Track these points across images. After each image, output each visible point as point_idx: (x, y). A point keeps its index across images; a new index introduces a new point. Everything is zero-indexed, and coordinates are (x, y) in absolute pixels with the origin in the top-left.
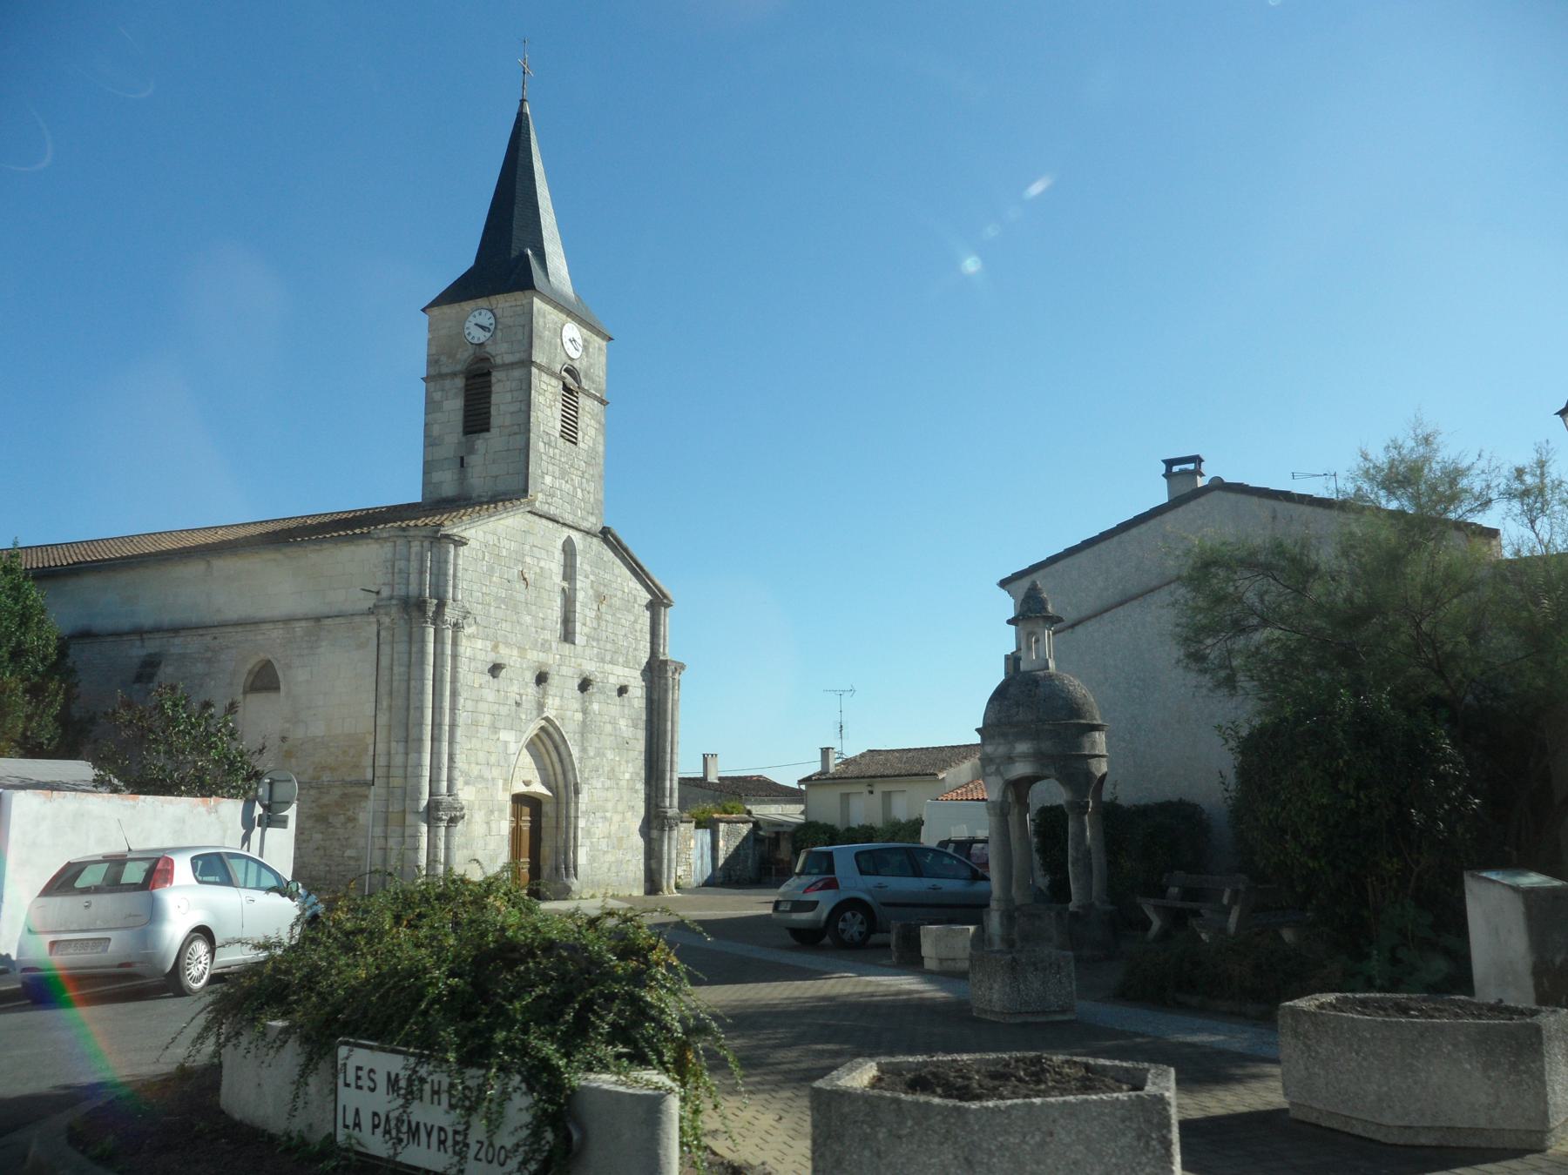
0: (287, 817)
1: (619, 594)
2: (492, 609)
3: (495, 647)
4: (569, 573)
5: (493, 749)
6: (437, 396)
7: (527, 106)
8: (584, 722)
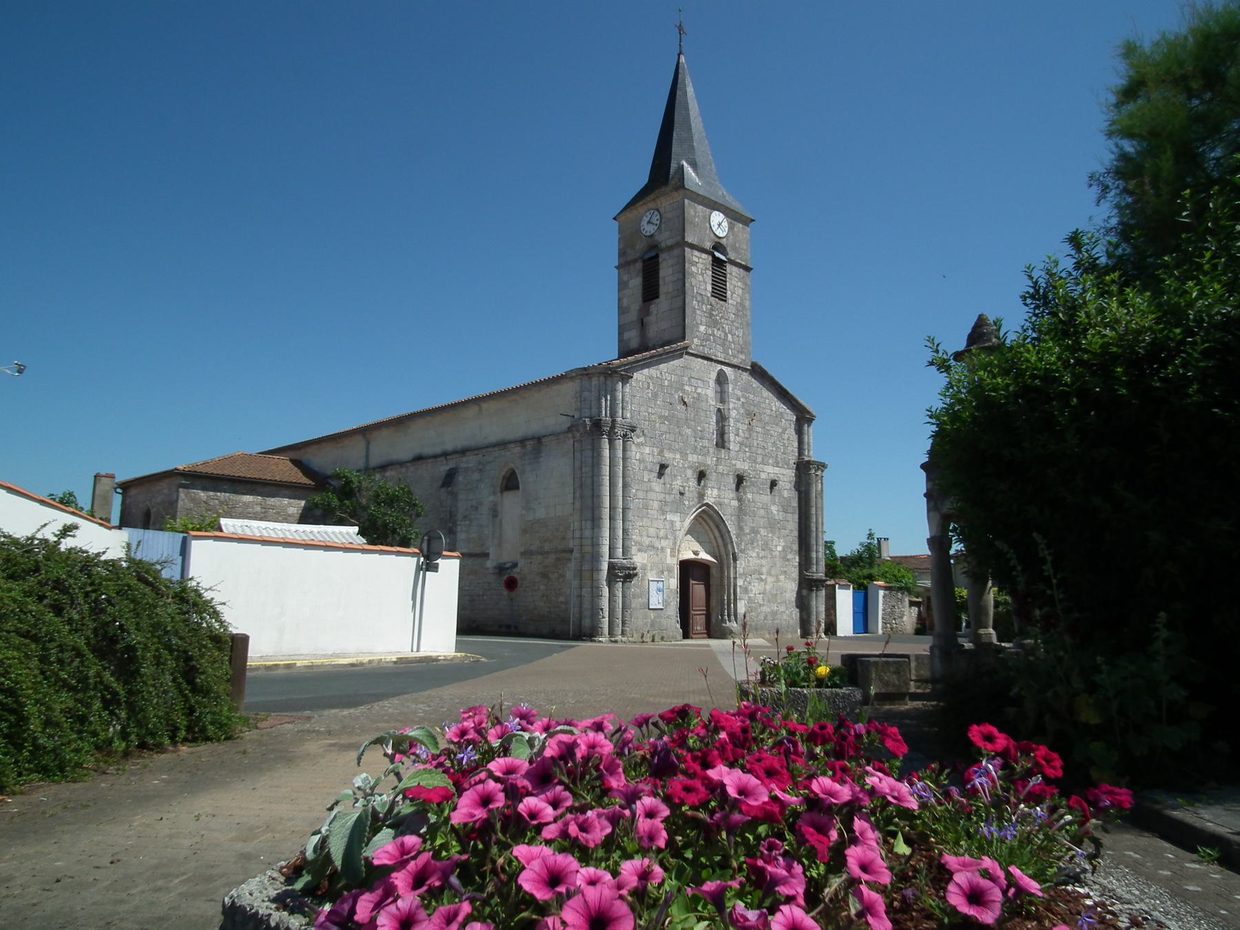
0: (438, 564)
1: (768, 412)
2: (657, 425)
3: (661, 453)
4: (722, 396)
5: (661, 526)
6: (625, 278)
7: (683, 59)
8: (740, 509)
